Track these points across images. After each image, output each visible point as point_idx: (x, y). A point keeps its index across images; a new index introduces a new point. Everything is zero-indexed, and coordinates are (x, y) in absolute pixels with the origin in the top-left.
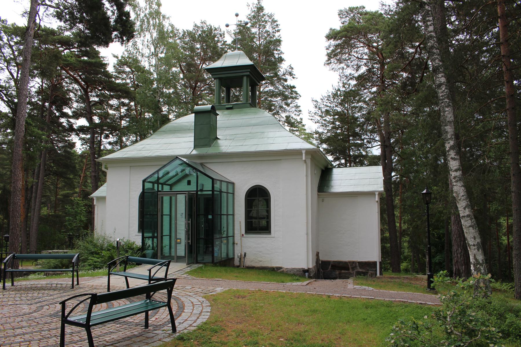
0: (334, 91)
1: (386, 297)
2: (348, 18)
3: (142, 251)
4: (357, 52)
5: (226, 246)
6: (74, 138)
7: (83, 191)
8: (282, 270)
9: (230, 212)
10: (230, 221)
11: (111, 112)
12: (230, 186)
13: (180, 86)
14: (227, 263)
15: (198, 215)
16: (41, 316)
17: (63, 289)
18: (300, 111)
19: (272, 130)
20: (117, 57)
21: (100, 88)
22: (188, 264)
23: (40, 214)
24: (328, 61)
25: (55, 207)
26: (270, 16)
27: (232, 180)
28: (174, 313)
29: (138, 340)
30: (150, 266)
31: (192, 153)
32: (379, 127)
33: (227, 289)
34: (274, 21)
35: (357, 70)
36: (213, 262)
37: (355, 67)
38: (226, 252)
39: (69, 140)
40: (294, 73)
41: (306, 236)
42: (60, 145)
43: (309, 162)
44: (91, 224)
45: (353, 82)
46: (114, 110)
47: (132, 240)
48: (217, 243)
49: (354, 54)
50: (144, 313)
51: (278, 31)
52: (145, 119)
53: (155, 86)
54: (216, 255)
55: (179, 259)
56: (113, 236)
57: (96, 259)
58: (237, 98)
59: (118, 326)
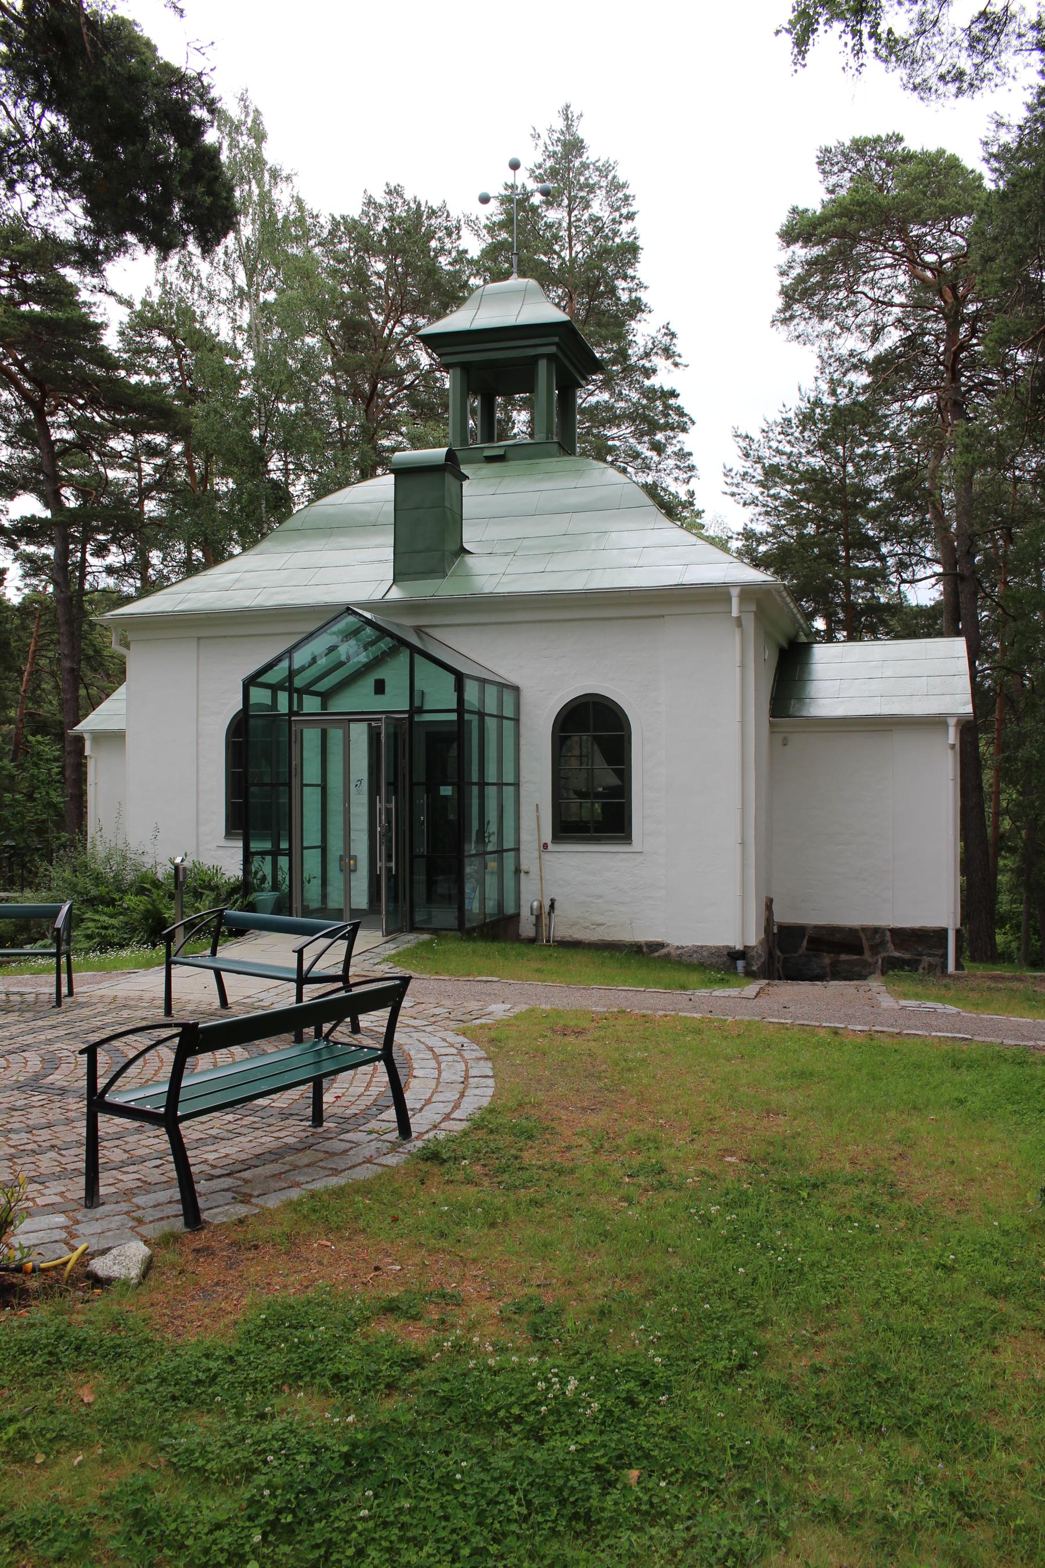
0: (804, 406)
1: (1006, 1036)
2: (847, 175)
3: (245, 896)
4: (873, 284)
5: (495, 879)
7: (31, 715)
8: (664, 951)
9: (509, 778)
10: (491, 805)
12: (508, 697)
14: (500, 929)
18: (692, 468)
19: (632, 526)
20: (129, 304)
21: (81, 402)
22: (388, 933)
24: (783, 311)
26: (604, 170)
27: (513, 679)
29: (306, 1161)
31: (389, 596)
32: (939, 516)
33: (524, 1007)
34: (616, 186)
35: (874, 340)
37: (868, 330)
40: (677, 350)
41: (738, 847)
43: (749, 622)
45: (862, 379)
49: (866, 290)
51: (630, 217)
53: (245, 393)
59: (230, 1117)
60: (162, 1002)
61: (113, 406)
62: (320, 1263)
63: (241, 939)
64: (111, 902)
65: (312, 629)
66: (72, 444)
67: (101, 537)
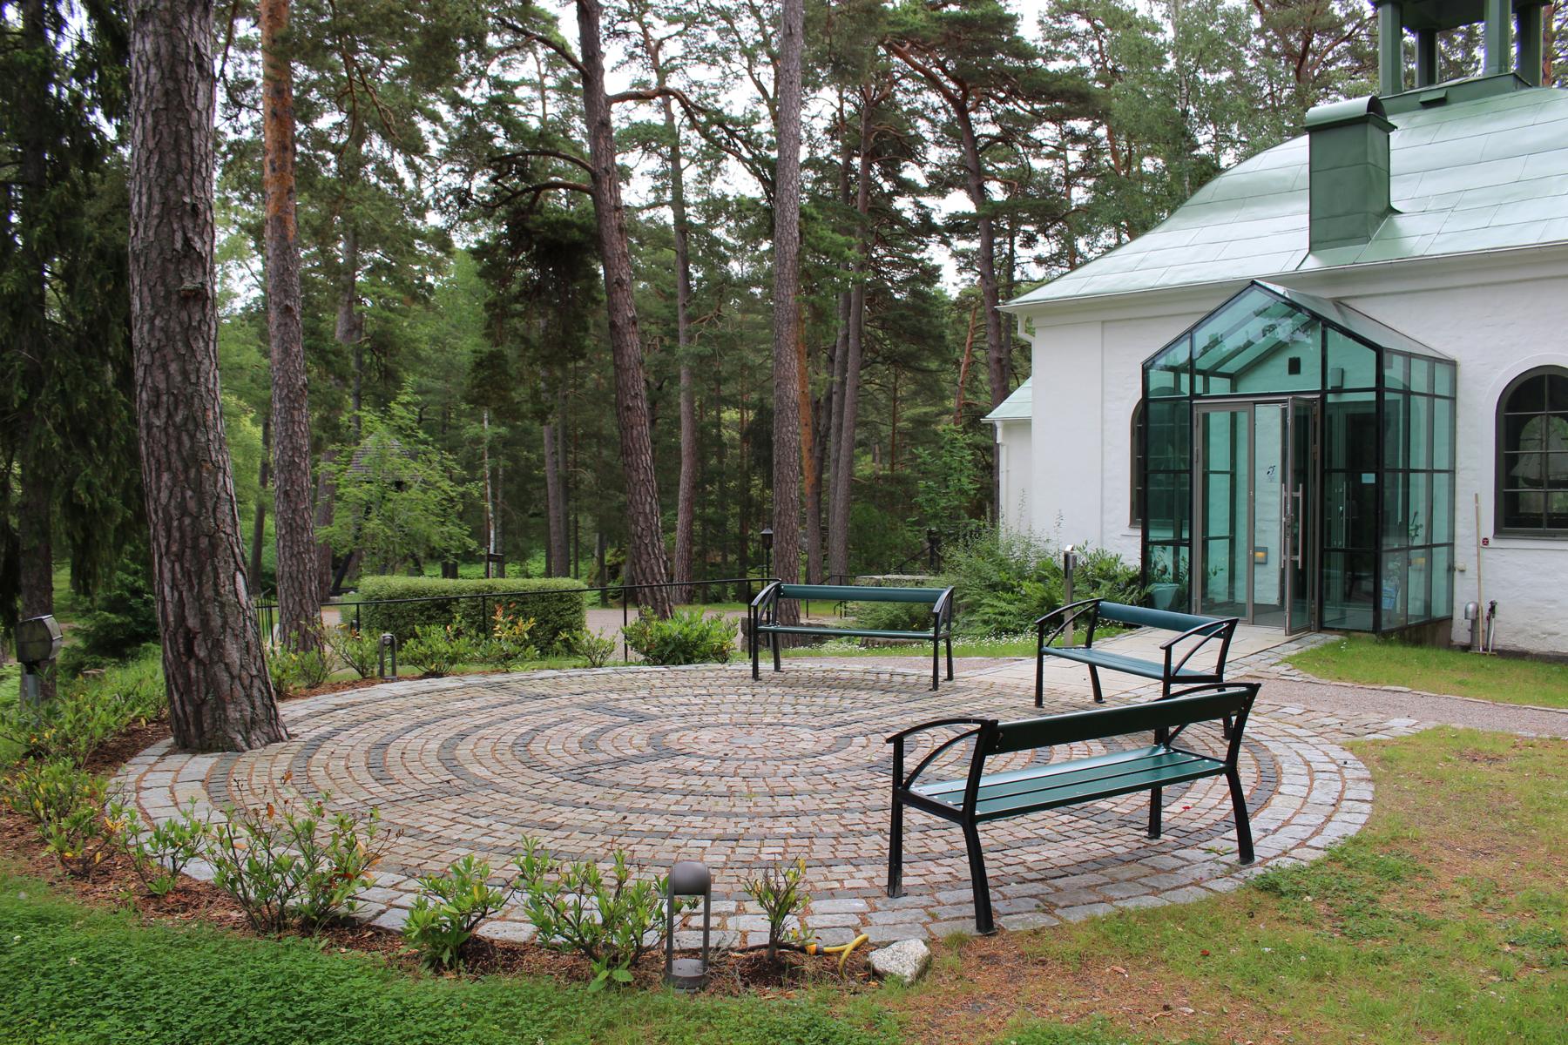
3: (1143, 586)
6: (935, 253)
7: (968, 405)
9: (1441, 462)
11: (1038, 164)
12: (1442, 373)
13: (1254, 57)
14: (1426, 631)
15: (1326, 472)
16: (845, 765)
17: (907, 689)
21: (1002, 95)
23: (851, 474)
25: (893, 454)
27: (1449, 352)
28: (1245, 793)
29: (1128, 875)
30: (1168, 635)
31: (1305, 267)
36: (1376, 628)
38: (1422, 595)
39: (922, 260)
42: (899, 276)
44: (992, 503)
46: (1049, 156)
47: (1112, 551)
48: (1391, 566)
50: (1148, 792)
52: (1142, 176)
53: (1170, 66)
54: (1386, 604)
55: (1261, 614)
56: (1053, 537)
57: (1003, 604)
58: (1457, 69)
59: (1065, 818)
60: (1033, 692)
61: (1032, 97)
62: (1106, 991)
63: (1136, 631)
64: (1010, 589)
65: (1212, 308)
66: (996, 139)
67: (1030, 228)
